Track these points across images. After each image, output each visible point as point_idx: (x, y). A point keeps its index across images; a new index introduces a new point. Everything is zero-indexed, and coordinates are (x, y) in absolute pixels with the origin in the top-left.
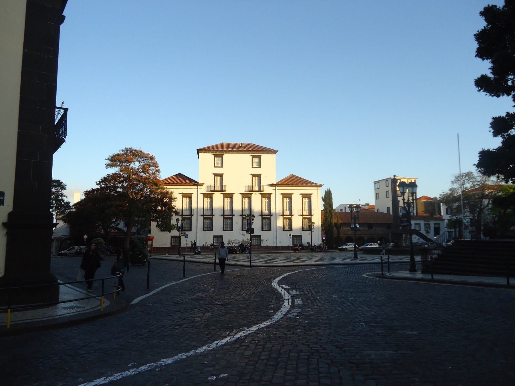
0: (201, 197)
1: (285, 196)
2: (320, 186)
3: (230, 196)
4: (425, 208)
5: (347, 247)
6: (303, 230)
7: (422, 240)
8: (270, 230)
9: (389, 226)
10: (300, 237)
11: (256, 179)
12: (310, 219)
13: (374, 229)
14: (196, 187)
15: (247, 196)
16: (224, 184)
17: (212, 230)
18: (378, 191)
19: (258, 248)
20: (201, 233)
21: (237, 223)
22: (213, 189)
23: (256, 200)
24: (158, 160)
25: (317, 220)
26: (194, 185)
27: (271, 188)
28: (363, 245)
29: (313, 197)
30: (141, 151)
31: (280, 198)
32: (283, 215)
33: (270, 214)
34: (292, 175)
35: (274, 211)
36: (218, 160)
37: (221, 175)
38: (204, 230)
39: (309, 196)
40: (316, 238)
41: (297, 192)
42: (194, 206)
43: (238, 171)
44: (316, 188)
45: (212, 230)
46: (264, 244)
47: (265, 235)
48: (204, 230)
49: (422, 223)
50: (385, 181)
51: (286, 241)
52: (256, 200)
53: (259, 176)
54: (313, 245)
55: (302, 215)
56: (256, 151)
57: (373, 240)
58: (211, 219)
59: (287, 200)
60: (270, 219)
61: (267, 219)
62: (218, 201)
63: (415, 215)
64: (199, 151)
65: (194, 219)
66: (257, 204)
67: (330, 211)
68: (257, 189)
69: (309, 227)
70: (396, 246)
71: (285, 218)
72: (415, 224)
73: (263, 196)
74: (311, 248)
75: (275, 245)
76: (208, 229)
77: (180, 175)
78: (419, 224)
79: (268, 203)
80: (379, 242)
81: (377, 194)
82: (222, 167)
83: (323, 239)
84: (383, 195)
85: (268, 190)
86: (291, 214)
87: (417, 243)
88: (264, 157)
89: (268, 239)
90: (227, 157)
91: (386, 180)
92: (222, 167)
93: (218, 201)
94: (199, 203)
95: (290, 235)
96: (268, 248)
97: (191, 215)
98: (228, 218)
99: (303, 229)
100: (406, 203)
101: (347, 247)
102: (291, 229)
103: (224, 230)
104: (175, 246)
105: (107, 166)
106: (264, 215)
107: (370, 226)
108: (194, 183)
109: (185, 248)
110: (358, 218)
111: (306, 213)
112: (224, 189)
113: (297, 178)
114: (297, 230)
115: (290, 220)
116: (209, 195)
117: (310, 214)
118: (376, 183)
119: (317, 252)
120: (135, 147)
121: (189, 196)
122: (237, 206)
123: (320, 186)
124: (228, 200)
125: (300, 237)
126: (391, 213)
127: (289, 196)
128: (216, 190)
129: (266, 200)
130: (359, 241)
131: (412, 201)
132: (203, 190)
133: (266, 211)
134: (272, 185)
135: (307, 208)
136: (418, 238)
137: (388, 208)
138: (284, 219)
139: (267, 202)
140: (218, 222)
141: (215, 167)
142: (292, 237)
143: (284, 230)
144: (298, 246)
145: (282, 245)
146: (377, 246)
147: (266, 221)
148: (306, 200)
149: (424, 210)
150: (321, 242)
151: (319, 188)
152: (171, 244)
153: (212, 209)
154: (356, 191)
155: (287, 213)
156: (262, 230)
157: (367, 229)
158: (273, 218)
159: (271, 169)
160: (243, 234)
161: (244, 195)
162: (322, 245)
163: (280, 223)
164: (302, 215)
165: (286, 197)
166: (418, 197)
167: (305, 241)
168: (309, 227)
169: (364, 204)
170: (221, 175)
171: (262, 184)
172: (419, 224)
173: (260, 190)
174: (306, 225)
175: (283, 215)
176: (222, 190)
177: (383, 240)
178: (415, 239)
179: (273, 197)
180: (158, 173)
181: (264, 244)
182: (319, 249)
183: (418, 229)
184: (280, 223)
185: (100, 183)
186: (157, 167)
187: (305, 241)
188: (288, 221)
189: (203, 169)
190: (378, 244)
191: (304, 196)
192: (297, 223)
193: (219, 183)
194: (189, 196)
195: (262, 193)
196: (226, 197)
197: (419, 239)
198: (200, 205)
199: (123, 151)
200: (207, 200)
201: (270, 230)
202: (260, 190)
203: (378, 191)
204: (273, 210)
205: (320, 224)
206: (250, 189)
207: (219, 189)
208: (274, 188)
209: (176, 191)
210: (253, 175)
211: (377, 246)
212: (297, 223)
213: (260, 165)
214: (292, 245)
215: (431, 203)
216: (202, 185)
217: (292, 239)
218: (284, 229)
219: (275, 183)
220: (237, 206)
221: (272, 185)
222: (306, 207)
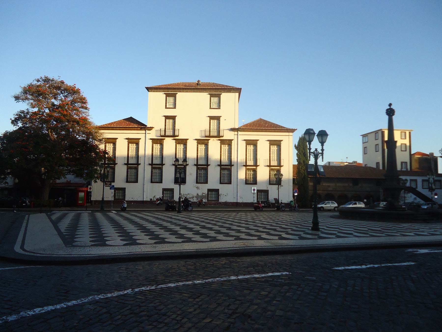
0: (149, 143)
1: (249, 142)
2: (292, 131)
3: (184, 142)
4: (420, 165)
5: (323, 205)
6: (270, 184)
7: (418, 200)
8: (230, 183)
9: (378, 182)
10: (266, 192)
11: (214, 123)
12: (279, 171)
14: (144, 132)
15: (203, 142)
16: (177, 128)
17: (207, 183)
18: (366, 145)
19: (215, 204)
20: (148, 186)
21: (191, 174)
22: (163, 134)
23: (214, 147)
24: (84, 93)
25: (287, 173)
26: (141, 129)
27: (233, 133)
29: (283, 144)
30: (62, 82)
32: (246, 166)
33: (231, 165)
34: (261, 119)
35: (236, 159)
37: (173, 118)
38: (152, 182)
39: (277, 143)
40: (286, 194)
41: (263, 139)
42: (141, 152)
43: (193, 114)
44: (287, 134)
45: (207, 183)
46: (222, 199)
47: (224, 189)
48: (152, 182)
49: (419, 179)
50: (374, 134)
51: (249, 195)
52: (214, 147)
53: (218, 118)
54: (280, 202)
55: (270, 166)
56: (215, 90)
57: (359, 199)
58: (161, 169)
60: (230, 170)
61: (227, 169)
62: (169, 147)
64: (149, 89)
65: (140, 168)
66: (215, 151)
67: (304, 162)
68: (216, 134)
69: (276, 180)
70: (390, 206)
71: (248, 169)
72: (423, 181)
73: (223, 142)
74: (278, 206)
75: (235, 201)
76: (157, 180)
77: (131, 120)
78: (416, 181)
79: (228, 151)
80: (365, 200)
81: (365, 149)
82: (175, 108)
83: (294, 196)
84: (371, 149)
85: (228, 135)
86: (256, 165)
87: (413, 203)
88: (224, 96)
89: (227, 194)
90: (180, 96)
91: (376, 132)
92: (175, 108)
93: (169, 147)
94: (146, 149)
95: (254, 190)
96: (226, 204)
97: (138, 164)
98: (180, 168)
101: (323, 205)
102: (255, 182)
103: (221, 183)
105: (17, 98)
106: (223, 165)
107: (355, 181)
108: (142, 127)
109: (96, 201)
110: (322, 154)
111: (274, 163)
112: (176, 134)
113: (266, 122)
114: (262, 183)
115: (255, 171)
116: (158, 141)
117: (280, 165)
118: (364, 136)
119: (284, 211)
120: (56, 75)
121: (136, 142)
122: (192, 153)
123: (292, 131)
124: (181, 147)
125: (266, 192)
126: (381, 168)
127: (253, 143)
128: (167, 134)
129: (225, 148)
130: (342, 199)
132: (152, 134)
133: (225, 160)
134: (233, 130)
135: (276, 158)
137: (378, 164)
139: (227, 150)
142: (256, 192)
143: (246, 184)
144: (264, 204)
147: (226, 172)
148: (274, 148)
149: (418, 167)
150: (291, 199)
151: (291, 134)
152: (115, 197)
153: (185, 160)
154: (344, 150)
155: (250, 162)
156: (221, 183)
157: (351, 185)
158: (233, 169)
159: (232, 111)
160: (198, 188)
161: (199, 142)
162: (293, 204)
163: (242, 174)
164: (270, 166)
166: (412, 153)
167: (272, 197)
168: (276, 180)
170: (173, 118)
171: (222, 128)
172: (416, 181)
174: (250, 177)
176: (174, 136)
177: (371, 199)
178: (410, 198)
179: (234, 144)
181: (222, 199)
182: (288, 207)
183: (414, 187)
184: (242, 174)
185: (14, 122)
187: (272, 197)
188: (252, 173)
189: (153, 110)
191: (272, 143)
192: (263, 174)
193: (171, 127)
194: (136, 142)
195: (221, 138)
196: (179, 143)
197: (415, 199)
198: (149, 152)
199: (38, 81)
202: (218, 136)
203: (366, 145)
204: (234, 158)
205: (291, 176)
207: (171, 134)
208: (236, 133)
209: (121, 137)
210: (211, 118)
211: (363, 206)
212: (263, 174)
214: (256, 201)
215: (426, 159)
216: (151, 129)
219: (237, 127)
220: (192, 153)
221: (233, 130)
222: (274, 156)
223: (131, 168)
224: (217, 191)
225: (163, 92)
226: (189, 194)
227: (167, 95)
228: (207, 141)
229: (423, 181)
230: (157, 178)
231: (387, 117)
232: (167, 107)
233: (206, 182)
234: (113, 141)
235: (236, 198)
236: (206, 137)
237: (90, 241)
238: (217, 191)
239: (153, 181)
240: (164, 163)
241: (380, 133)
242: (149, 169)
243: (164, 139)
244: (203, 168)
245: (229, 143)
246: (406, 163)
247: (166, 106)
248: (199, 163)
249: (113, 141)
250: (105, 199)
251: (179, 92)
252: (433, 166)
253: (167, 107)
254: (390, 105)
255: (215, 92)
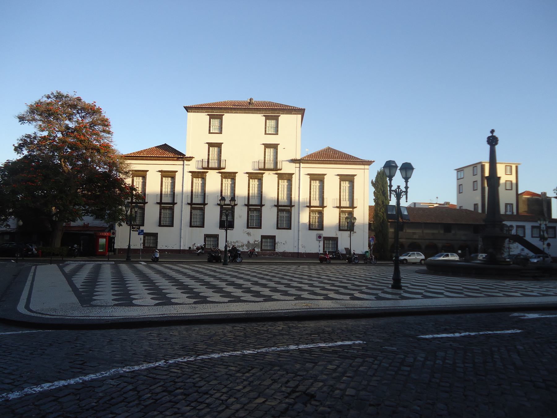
0: (188, 177)
1: (313, 177)
2: (369, 163)
3: (232, 176)
5: (406, 257)
6: (340, 230)
7: (526, 251)
8: (290, 228)
9: (476, 229)
11: (270, 152)
12: (351, 213)
13: (453, 232)
14: (181, 162)
15: (256, 176)
16: (223, 158)
18: (461, 182)
19: (270, 255)
20: (186, 230)
21: (240, 217)
22: (205, 165)
23: (270, 183)
25: (362, 215)
26: (178, 159)
27: (293, 165)
28: (433, 255)
31: (305, 180)
32: (310, 206)
33: (291, 206)
34: (329, 148)
35: (297, 198)
36: (215, 122)
38: (191, 226)
39: (350, 179)
40: (360, 243)
41: (332, 173)
42: (178, 188)
43: (244, 141)
44: (362, 167)
46: (280, 249)
47: (282, 236)
48: (191, 226)
49: (528, 226)
50: (471, 168)
52: (270, 183)
53: (275, 147)
55: (340, 207)
56: (272, 111)
58: (203, 210)
59: (316, 184)
60: (290, 212)
61: (285, 211)
62: (214, 183)
63: (515, 213)
65: (177, 208)
66: (271, 187)
67: (383, 202)
68: (272, 167)
69: (348, 224)
70: (491, 259)
71: (313, 211)
72: (533, 227)
73: (281, 176)
74: (349, 258)
75: (296, 251)
76: (167, 223)
77: (165, 147)
78: (523, 227)
79: (288, 188)
80: (460, 252)
81: (460, 186)
82: (221, 133)
84: (468, 187)
85: (287, 168)
86: (322, 206)
87: (519, 255)
88: (284, 118)
89: (286, 242)
90: (227, 117)
91: (474, 166)
92: (221, 133)
93: (214, 183)
94: (184, 184)
96: (285, 255)
97: (174, 203)
98: (227, 209)
99: (340, 228)
100: (395, 191)
101: (406, 257)
102: (321, 227)
104: (149, 247)
105: (22, 119)
108: (179, 156)
110: (406, 192)
111: (345, 203)
112: (222, 165)
113: (335, 152)
115: (321, 213)
116: (200, 175)
117: (352, 206)
118: (459, 170)
120: (70, 90)
121: (171, 175)
122: (241, 190)
123: (369, 163)
124: (228, 182)
127: (320, 178)
128: (210, 166)
129: (284, 184)
130: (431, 249)
131: (404, 190)
132: (192, 166)
133: (283, 198)
134: (294, 161)
135: (347, 197)
136: (521, 247)
137: (476, 205)
138: (311, 211)
140: (212, 215)
141: (210, 133)
144: (332, 255)
145: (308, 251)
146: (455, 258)
149: (526, 209)
150: (367, 249)
151: (367, 167)
154: (433, 188)
156: (278, 228)
157: (442, 232)
158: (294, 211)
161: (251, 176)
162: (368, 255)
163: (304, 217)
164: (340, 207)
165: (316, 180)
166: (520, 192)
167: (342, 247)
168: (348, 224)
169: (443, 203)
172: (523, 227)
173: (275, 169)
175: (310, 206)
176: (219, 168)
177: (467, 250)
178: (516, 249)
180: (105, 135)
181: (280, 249)
182: (363, 259)
183: (521, 234)
184: (304, 217)
185: (18, 149)
186: (107, 126)
187: (342, 247)
188: (317, 215)
189: (194, 136)
190: (459, 255)
191: (343, 178)
192: (331, 218)
193: (216, 157)
194: (171, 175)
195: (279, 172)
197: (523, 250)
198: (187, 188)
199: (48, 97)
200: (198, 182)
201: (290, 228)
202: (275, 169)
203: (461, 182)
204: (295, 197)
205: (367, 220)
206: (262, 166)
208: (298, 165)
209: (153, 169)
210: (267, 146)
212: (331, 218)
213: (277, 131)
214: (322, 252)
215: (537, 200)
216: (190, 159)
217: (322, 243)
218: (311, 227)
219: (299, 158)
220: (241, 190)
221: (294, 161)
222: (346, 195)
223: (164, 208)
224: (273, 238)
225: (206, 112)
226: (237, 242)
227: (211, 117)
228: (261, 175)
229: (533, 227)
230: (197, 221)
231: (488, 147)
232: (211, 131)
233: (259, 227)
234: (143, 174)
235: (297, 247)
236: (260, 169)
237: (113, 291)
238: (273, 238)
239: (193, 225)
240: (175, 202)
241: (479, 167)
242: (187, 210)
243: (207, 172)
244: (255, 209)
245: (288, 177)
246: (512, 204)
247: (210, 130)
248: (250, 203)
249: (143, 174)
250: (132, 247)
251: (226, 113)
252: (545, 209)
253: (211, 131)
254: (492, 131)
255: (272, 113)
